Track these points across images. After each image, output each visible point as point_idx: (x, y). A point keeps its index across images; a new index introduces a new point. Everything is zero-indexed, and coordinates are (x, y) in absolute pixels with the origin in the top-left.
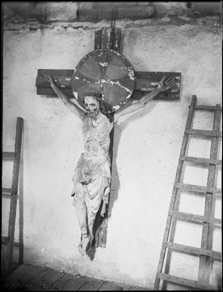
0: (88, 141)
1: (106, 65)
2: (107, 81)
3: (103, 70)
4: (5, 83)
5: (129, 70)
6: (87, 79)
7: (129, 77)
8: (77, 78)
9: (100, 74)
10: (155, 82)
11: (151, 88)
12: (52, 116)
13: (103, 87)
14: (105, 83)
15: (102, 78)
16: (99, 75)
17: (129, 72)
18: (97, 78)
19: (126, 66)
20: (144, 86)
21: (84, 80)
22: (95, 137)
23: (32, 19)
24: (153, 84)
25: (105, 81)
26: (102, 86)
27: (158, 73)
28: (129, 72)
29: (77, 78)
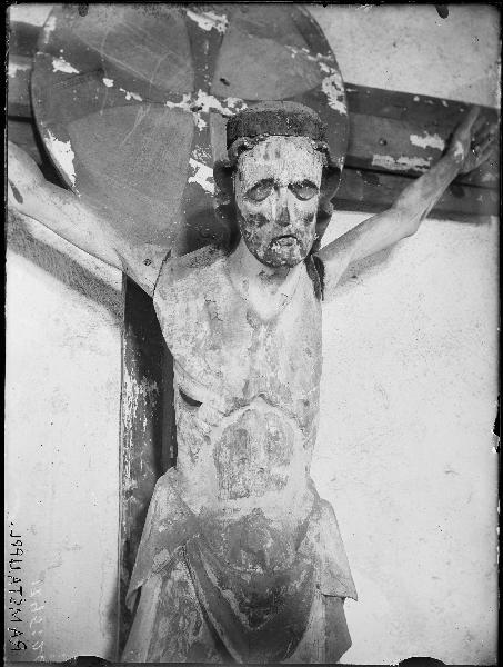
0: (240, 404)
1: (221, 28)
2: (224, 105)
3: (203, 49)
4: (488, 410)
5: (325, 68)
6: (124, 81)
7: (324, 98)
8: (61, 66)
9: (188, 64)
10: (424, 136)
11: (411, 157)
12: (219, 82)
13: (207, 130)
14: (213, 110)
15: (201, 84)
16: (182, 76)
17: (324, 75)
18: (173, 83)
19: (309, 45)
20: (385, 146)
21: (109, 83)
22: (282, 377)
23: (201, 591)
24: (415, 140)
25: (216, 104)
26: (202, 124)
27: (423, 98)
28: (324, 75)
29: (61, 66)
